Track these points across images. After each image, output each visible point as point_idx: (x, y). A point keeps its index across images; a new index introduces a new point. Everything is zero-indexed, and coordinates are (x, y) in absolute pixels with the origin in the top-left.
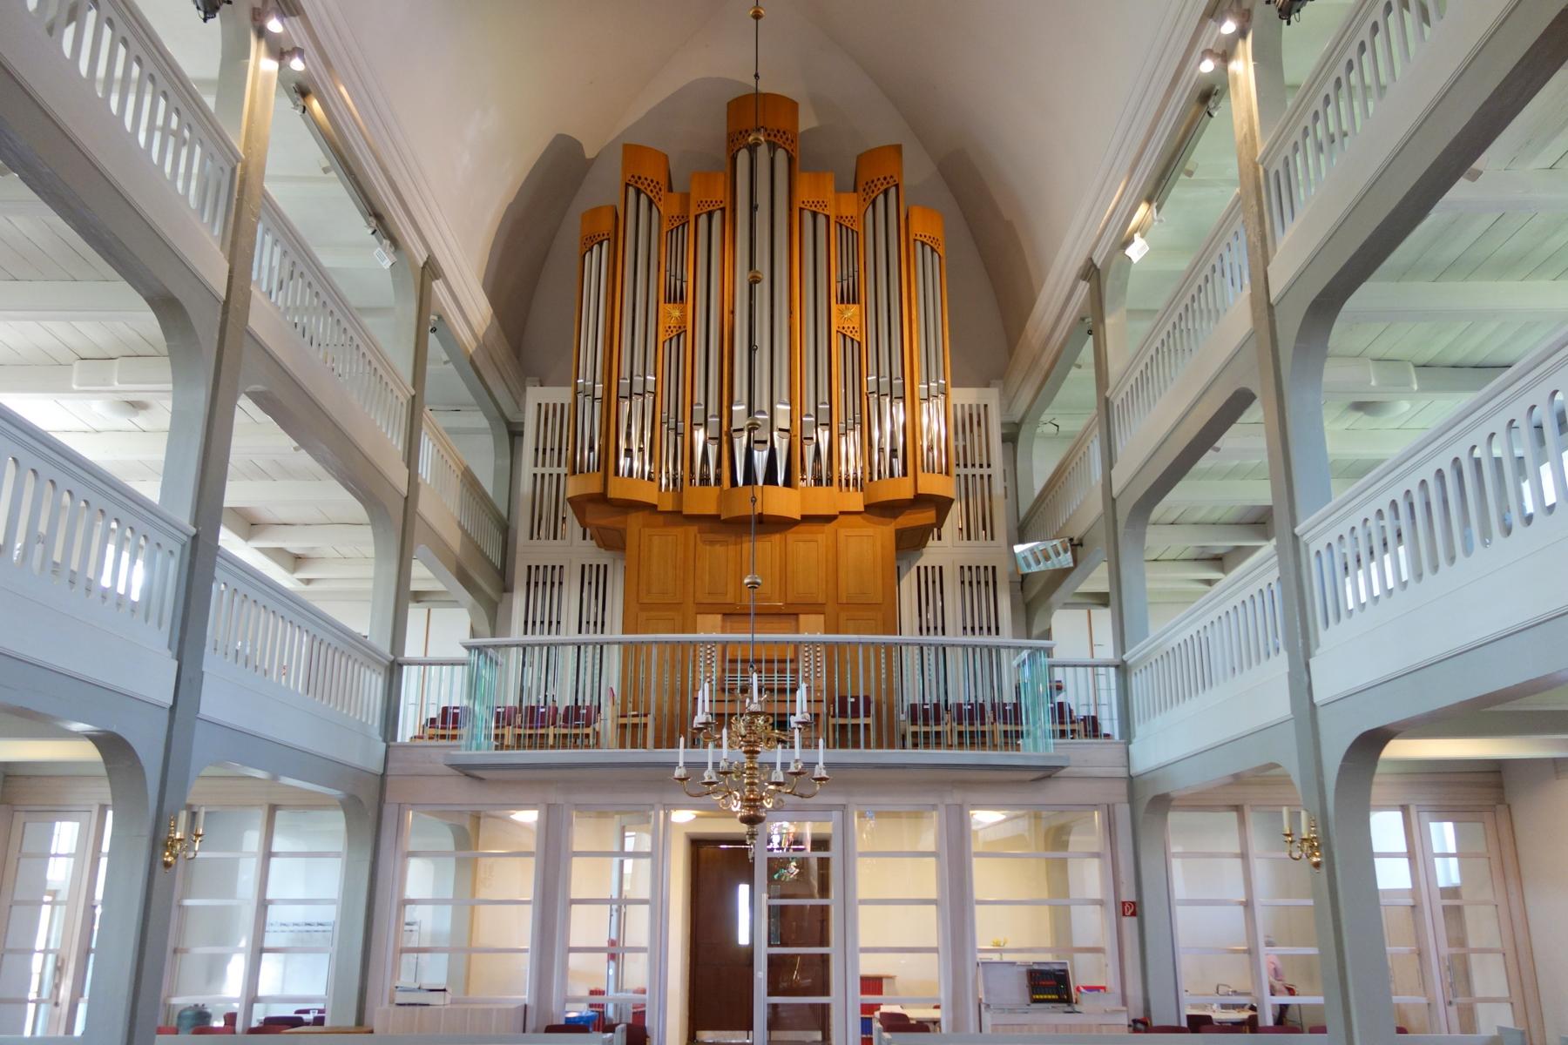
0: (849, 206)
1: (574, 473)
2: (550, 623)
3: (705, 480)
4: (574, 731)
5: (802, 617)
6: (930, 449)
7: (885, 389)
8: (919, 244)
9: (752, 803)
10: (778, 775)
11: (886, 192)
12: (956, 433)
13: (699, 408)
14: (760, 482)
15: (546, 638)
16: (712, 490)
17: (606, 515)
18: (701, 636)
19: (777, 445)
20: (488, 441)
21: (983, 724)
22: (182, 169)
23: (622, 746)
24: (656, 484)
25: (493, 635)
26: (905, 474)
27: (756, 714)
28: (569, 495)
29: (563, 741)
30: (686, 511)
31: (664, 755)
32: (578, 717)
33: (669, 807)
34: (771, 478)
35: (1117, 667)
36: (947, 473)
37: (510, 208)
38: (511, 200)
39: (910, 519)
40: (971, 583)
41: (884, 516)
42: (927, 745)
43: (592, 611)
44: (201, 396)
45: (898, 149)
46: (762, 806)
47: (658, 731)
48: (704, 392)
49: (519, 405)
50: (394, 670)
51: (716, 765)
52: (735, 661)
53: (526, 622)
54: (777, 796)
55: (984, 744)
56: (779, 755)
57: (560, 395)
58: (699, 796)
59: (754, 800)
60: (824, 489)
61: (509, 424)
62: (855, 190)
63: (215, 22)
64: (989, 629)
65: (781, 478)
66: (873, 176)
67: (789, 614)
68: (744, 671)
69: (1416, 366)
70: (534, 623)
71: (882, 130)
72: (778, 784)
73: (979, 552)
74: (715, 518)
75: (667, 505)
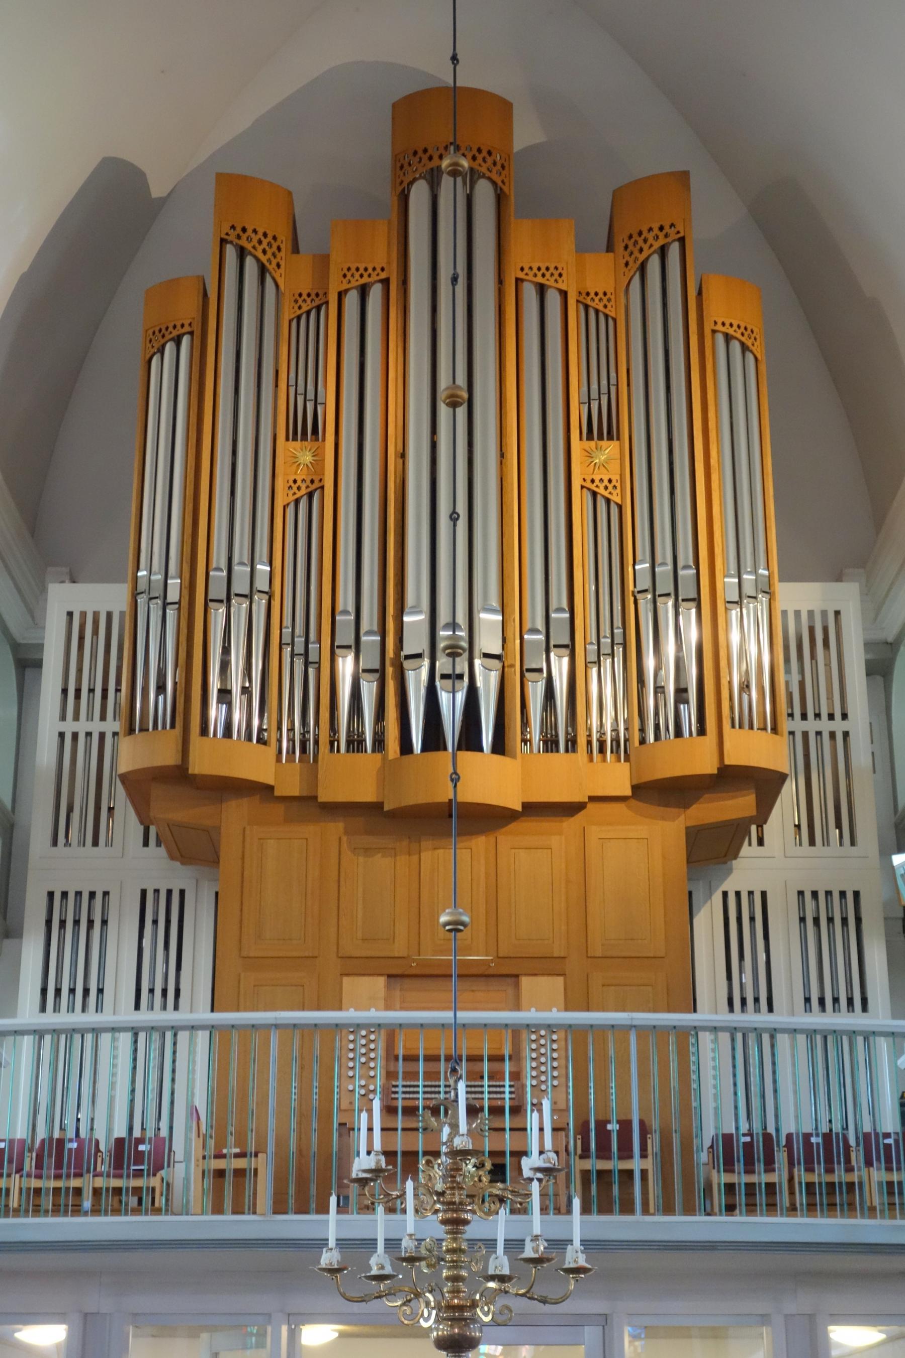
0: (600, 275)
1: (131, 731)
2: (86, 991)
3: (356, 743)
4: (134, 1183)
5: (525, 981)
6: (745, 687)
8: (720, 338)
9: (457, 1313)
10: (500, 1263)
11: (663, 252)
12: (787, 660)
13: (346, 620)
15: (78, 1018)
16: (369, 760)
17: (184, 804)
18: (349, 1015)
19: (479, 683)
21: (849, 1169)
23: (218, 1209)
24: (272, 749)
26: (702, 731)
27: (464, 1154)
28: (123, 768)
29: (110, 1201)
30: (324, 796)
31: (294, 1225)
32: (136, 1158)
33: (297, 1319)
34: (470, 739)
36: (775, 730)
37: (25, 280)
38: (25, 268)
39: (711, 811)
40: (816, 921)
41: (667, 805)
42: (751, 1208)
43: (158, 972)
45: (683, 177)
46: (474, 1320)
47: (280, 1180)
48: (353, 592)
49: (35, 612)
51: (392, 1244)
52: (415, 1059)
53: (44, 991)
54: (501, 1301)
55: (851, 1205)
56: (501, 1225)
57: (108, 598)
58: (362, 1300)
59: (461, 1308)
60: (561, 757)
62: (610, 248)
64: (850, 1001)
66: (641, 226)
67: (502, 976)
68: (432, 1075)
70: (58, 992)
71: (652, 146)
72: (501, 1279)
73: (832, 866)
74: (376, 808)
75: (290, 784)
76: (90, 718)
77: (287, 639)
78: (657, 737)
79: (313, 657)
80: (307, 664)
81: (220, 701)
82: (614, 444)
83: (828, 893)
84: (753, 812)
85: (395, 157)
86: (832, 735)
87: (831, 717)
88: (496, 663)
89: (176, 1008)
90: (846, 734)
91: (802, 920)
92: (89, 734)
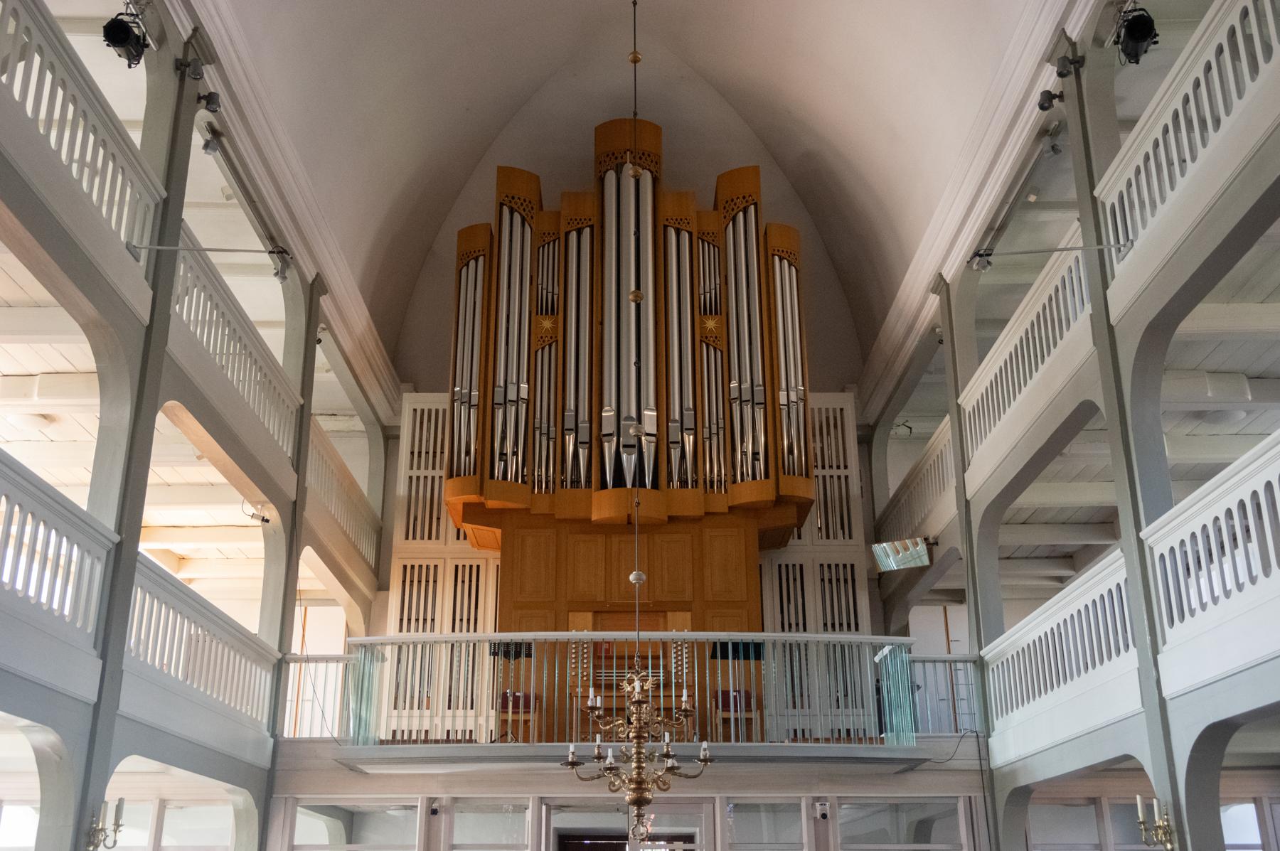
1: (450, 476)
5: (669, 614)
6: (791, 451)
7: (746, 396)
8: (777, 258)
11: (745, 211)
13: (570, 414)
14: (629, 485)
18: (573, 635)
20: (362, 444)
22: (106, 198)
25: (368, 634)
26: (767, 476)
35: (975, 662)
36: (807, 475)
40: (830, 581)
44: (125, 413)
45: (756, 169)
48: (577, 399)
49: (397, 412)
50: (280, 669)
53: (401, 620)
61: (384, 429)
63: (141, 68)
64: (849, 625)
65: (648, 480)
66: (734, 195)
69: (1250, 378)
76: (426, 468)
77: (537, 425)
78: (742, 480)
79: (552, 435)
80: (548, 439)
81: (500, 460)
82: (718, 317)
83: (837, 566)
84: (796, 521)
85: (597, 157)
86: (839, 477)
87: (838, 467)
88: (653, 439)
89: (475, 630)
90: (846, 477)
91: (823, 580)
92: (426, 477)
